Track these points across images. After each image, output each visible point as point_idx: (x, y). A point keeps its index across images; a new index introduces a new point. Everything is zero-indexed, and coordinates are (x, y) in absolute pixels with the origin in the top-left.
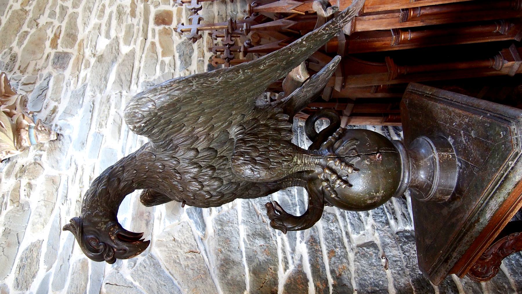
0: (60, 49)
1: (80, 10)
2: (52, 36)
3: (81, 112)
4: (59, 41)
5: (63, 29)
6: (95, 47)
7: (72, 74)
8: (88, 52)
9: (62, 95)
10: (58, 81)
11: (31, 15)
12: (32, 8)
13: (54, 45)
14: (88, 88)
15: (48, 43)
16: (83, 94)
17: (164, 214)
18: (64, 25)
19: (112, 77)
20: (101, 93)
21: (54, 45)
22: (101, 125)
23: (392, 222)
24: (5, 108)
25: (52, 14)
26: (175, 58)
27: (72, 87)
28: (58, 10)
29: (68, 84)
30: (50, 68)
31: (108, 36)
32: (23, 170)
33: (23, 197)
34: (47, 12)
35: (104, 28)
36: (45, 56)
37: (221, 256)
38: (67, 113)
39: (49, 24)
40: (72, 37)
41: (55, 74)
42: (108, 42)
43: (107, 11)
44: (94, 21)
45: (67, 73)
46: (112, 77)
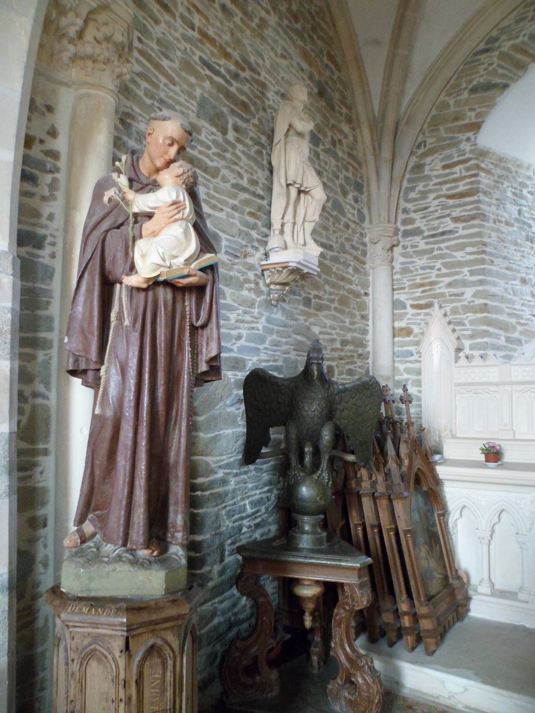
0: (313, 301)
1: (333, 312)
2: (320, 295)
3: (284, 319)
4: (317, 300)
5: (498, 316)
6: (315, 325)
7: (302, 310)
8: (312, 320)
9: (292, 305)
10: (298, 301)
11: (330, 279)
12: (333, 279)
13: (316, 297)
14: (294, 322)
15: (316, 292)
16: (292, 320)
17: (237, 377)
18: (325, 302)
19: (299, 338)
20: (293, 331)
21: (316, 297)
22: (278, 332)
23: (229, 541)
24: (461, 211)
25: (331, 294)
26: (491, 546)
27: (295, 311)
28: (332, 297)
29: (296, 308)
30: (304, 295)
31: (321, 333)
32: (257, 284)
33: (247, 285)
34: (331, 290)
35: (324, 330)
36: (310, 291)
37: (208, 119)
38: (284, 309)
39: (325, 291)
40: (320, 308)
41: (301, 298)
42: (317, 333)
43: (333, 332)
44: (328, 322)
45: (301, 307)
46: (299, 338)
